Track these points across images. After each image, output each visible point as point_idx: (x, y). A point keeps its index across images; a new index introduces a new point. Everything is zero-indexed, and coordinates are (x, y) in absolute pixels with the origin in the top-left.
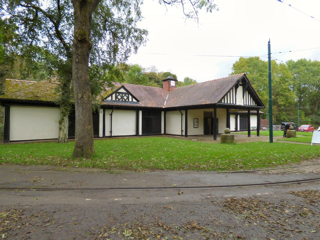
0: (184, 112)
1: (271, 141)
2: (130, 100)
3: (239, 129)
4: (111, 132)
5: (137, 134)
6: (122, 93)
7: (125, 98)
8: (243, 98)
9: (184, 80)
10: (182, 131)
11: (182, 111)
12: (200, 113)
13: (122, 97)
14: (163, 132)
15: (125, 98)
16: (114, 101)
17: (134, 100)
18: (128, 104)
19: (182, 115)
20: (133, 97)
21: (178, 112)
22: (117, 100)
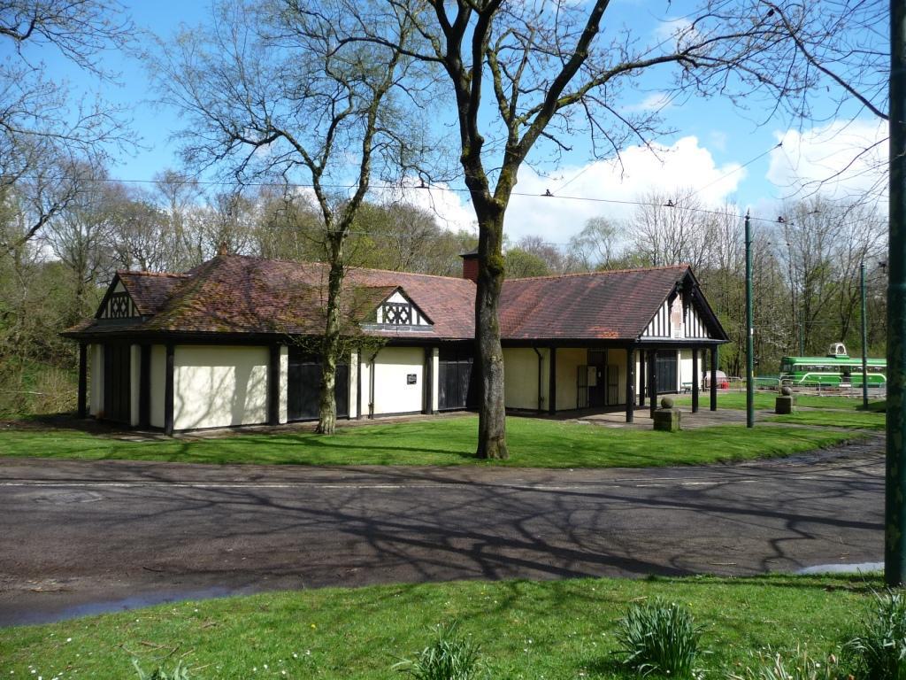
0: (546, 353)
1: (750, 424)
2: (414, 322)
3: (435, 406)
4: (371, 406)
5: (427, 409)
6: (397, 305)
7: (404, 316)
8: (685, 322)
9: (445, 233)
10: (540, 400)
11: (540, 350)
12: (581, 355)
13: (398, 315)
14: (638, 404)
15: (404, 316)
16: (380, 327)
17: (423, 322)
18: (383, 330)
19: (541, 359)
20: (421, 313)
21: (531, 351)
22: (387, 322)
